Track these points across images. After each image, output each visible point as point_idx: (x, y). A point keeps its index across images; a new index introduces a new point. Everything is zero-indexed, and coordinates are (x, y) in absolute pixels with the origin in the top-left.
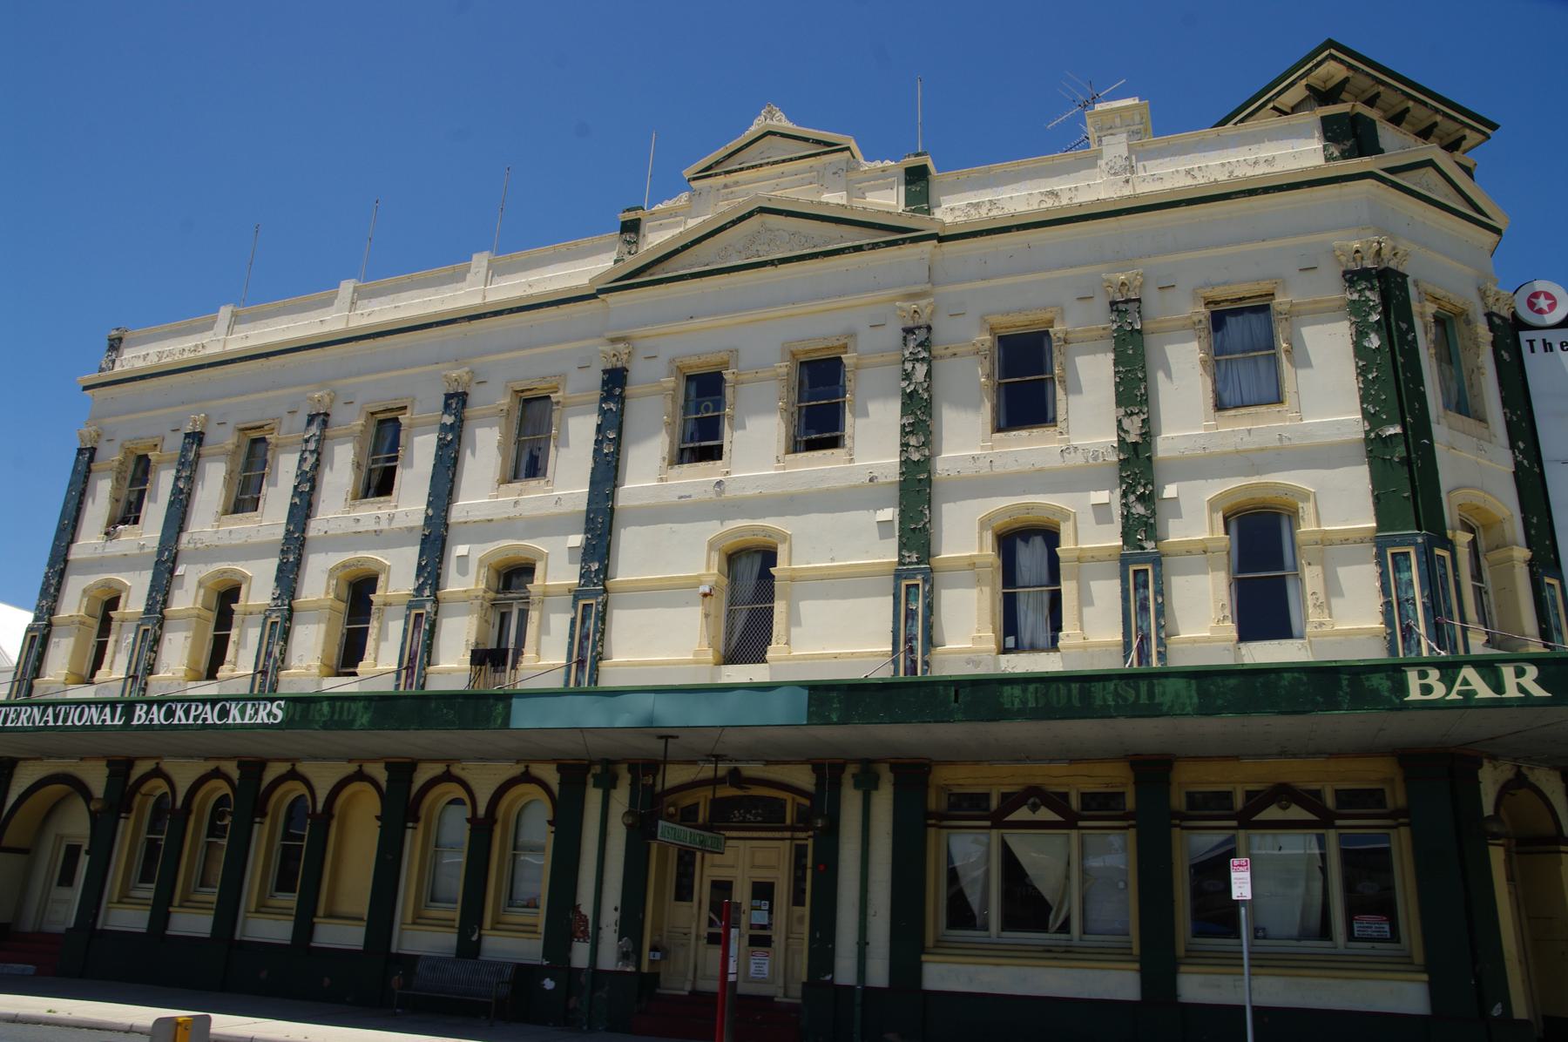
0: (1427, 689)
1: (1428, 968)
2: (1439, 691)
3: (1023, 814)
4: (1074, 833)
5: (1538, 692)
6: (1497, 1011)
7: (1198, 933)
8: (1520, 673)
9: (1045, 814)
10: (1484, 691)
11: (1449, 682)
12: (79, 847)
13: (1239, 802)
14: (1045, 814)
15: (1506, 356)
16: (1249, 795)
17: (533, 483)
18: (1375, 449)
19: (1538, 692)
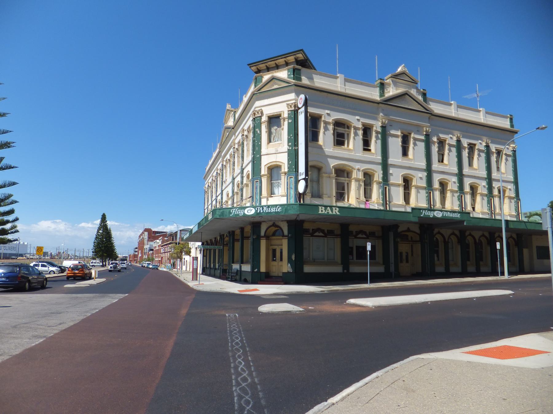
0: (322, 211)
1: (342, 264)
2: (324, 211)
3: (317, 234)
4: (326, 239)
5: (338, 213)
6: (256, 270)
7: (357, 259)
8: (336, 209)
9: (321, 234)
10: (330, 213)
11: (325, 210)
12: (223, 235)
13: (311, 231)
14: (364, 236)
15: (259, 132)
16: (356, 232)
17: (456, 106)
18: (289, 152)
19: (338, 213)
